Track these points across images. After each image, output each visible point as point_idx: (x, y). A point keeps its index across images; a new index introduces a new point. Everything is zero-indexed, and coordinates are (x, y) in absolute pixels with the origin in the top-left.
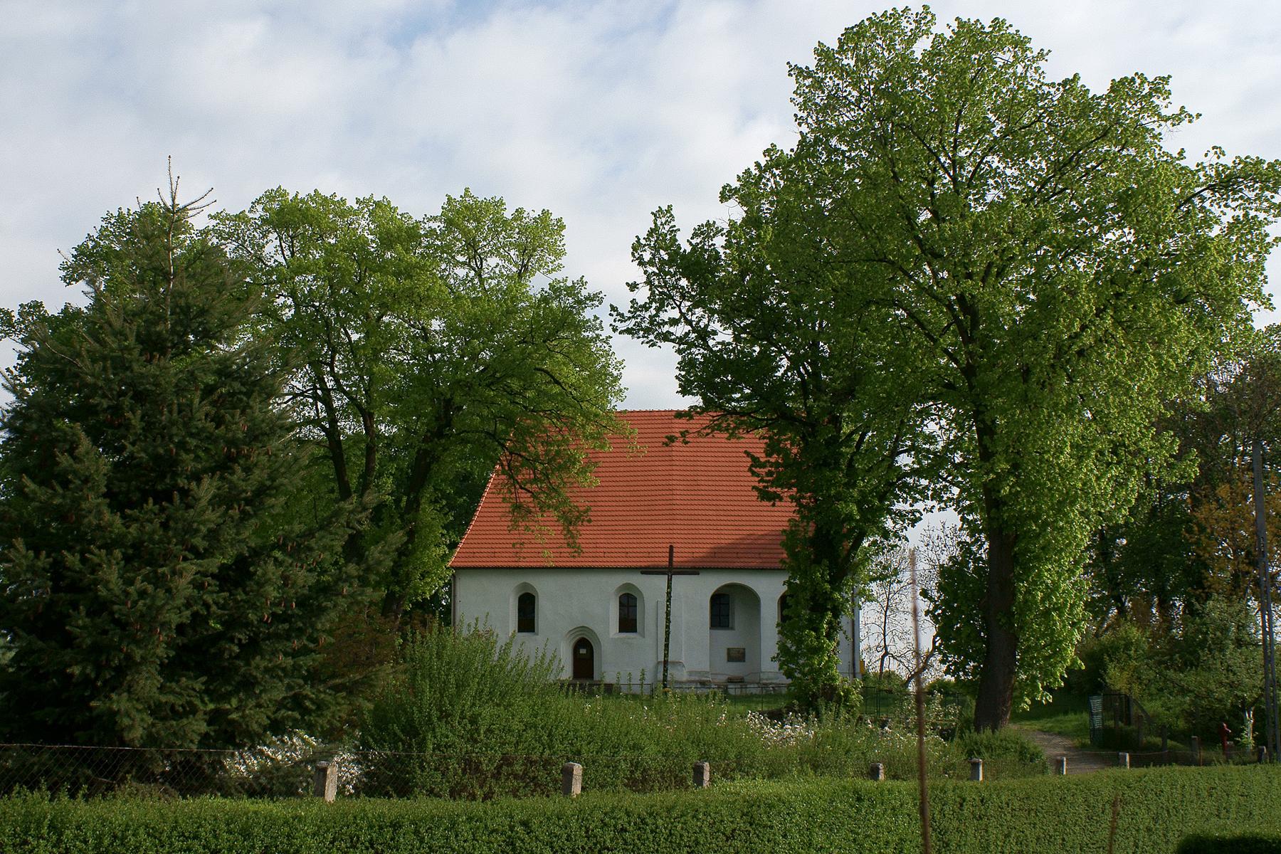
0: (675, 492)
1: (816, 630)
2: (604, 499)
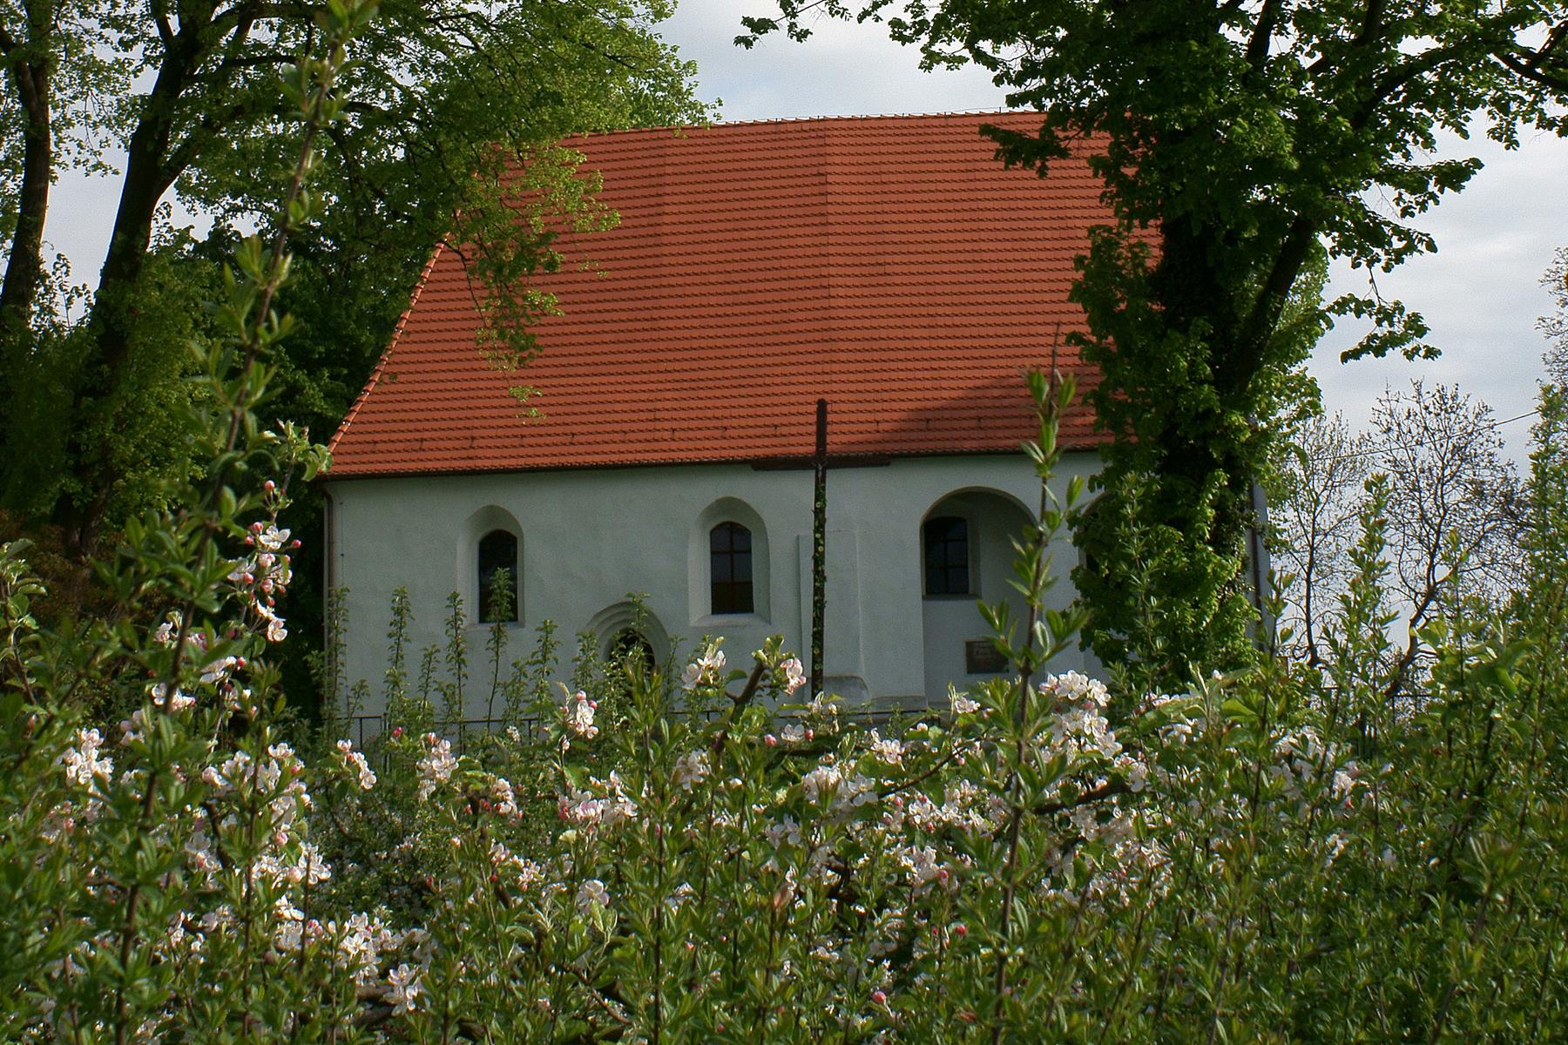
0: (833, 292)
1: (1183, 524)
2: (671, 313)
